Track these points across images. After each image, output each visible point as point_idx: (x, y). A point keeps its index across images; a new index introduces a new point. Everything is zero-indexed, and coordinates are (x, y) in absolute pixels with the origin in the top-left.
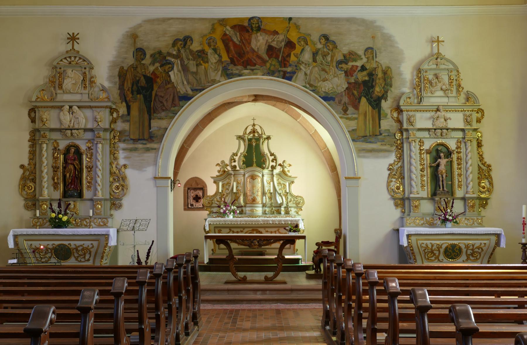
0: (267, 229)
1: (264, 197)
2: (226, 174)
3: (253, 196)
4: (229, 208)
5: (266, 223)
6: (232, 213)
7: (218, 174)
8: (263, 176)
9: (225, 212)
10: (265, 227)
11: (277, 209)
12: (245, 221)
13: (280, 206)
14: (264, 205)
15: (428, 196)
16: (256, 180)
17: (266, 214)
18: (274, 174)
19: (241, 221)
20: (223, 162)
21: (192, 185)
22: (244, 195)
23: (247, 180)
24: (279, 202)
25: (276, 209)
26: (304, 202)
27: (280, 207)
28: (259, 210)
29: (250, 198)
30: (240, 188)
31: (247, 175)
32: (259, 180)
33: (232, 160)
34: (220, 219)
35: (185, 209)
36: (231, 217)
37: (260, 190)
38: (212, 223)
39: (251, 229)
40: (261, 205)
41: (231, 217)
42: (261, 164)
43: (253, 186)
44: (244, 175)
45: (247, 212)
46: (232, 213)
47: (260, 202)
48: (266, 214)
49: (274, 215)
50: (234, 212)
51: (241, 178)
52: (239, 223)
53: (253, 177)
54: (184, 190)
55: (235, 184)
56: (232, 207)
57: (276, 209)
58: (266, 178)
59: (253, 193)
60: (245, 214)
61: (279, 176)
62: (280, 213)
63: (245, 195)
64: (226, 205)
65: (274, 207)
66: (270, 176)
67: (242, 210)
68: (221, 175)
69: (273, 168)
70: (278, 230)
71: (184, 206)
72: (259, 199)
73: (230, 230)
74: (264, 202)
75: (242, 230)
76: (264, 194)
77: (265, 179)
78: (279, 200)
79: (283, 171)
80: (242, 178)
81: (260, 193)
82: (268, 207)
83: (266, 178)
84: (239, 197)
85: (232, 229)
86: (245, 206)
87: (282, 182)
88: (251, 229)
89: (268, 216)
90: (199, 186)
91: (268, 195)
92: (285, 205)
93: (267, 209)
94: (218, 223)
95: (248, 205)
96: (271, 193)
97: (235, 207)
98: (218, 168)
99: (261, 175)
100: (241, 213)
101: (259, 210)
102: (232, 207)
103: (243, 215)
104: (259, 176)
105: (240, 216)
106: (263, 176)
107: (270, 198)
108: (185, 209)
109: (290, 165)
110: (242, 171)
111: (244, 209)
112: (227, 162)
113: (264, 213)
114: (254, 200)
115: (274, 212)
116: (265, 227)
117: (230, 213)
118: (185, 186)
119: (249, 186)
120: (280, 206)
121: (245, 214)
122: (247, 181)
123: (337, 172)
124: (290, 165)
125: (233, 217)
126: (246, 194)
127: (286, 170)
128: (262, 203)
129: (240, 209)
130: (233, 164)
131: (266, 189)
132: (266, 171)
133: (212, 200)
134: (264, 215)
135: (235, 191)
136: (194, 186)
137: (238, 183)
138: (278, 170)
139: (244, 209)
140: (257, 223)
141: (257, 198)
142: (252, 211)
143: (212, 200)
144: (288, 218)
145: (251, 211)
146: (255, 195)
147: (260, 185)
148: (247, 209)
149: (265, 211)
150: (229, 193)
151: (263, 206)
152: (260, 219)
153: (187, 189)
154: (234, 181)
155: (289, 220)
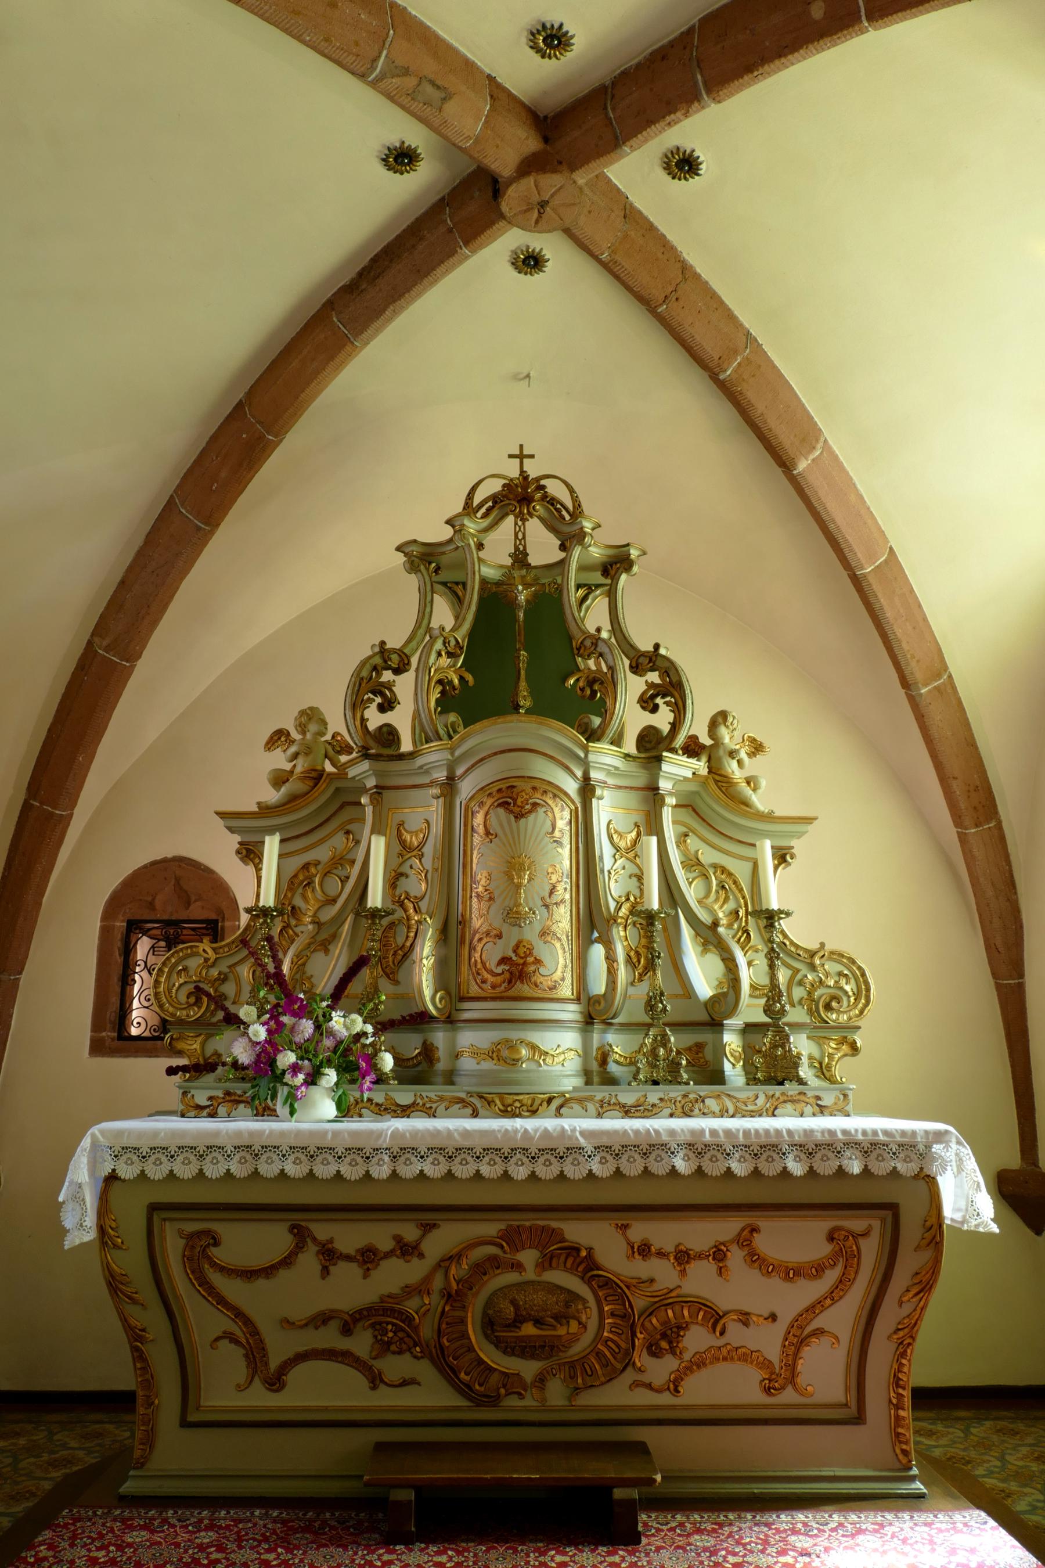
0: (641, 1230)
1: (598, 951)
2: (324, 793)
3: (512, 936)
4: (307, 1027)
5: (633, 1168)
6: (331, 1076)
7: (272, 796)
8: (587, 789)
9: (265, 1063)
10: (623, 1212)
11: (685, 1048)
12: (441, 1150)
13: (713, 1017)
14: (594, 1013)
15: (209, 1058)
16: (537, 821)
17: (610, 1081)
18: (665, 785)
19: (401, 1151)
20: (310, 716)
21: (151, 906)
22: (444, 934)
23: (469, 814)
24: (704, 987)
25: (689, 1039)
26: (863, 990)
27: (716, 1025)
28: (559, 1051)
29: (490, 953)
30: (415, 885)
31: (466, 788)
32: (563, 818)
33: (370, 686)
34: (242, 1125)
35: (98, 1048)
36: (321, 1107)
37: (564, 892)
38: (127, 1172)
39: (491, 1229)
40: (571, 1012)
41: (321, 1107)
42: (584, 708)
43: (514, 867)
44: (450, 785)
45: (467, 1064)
46: (331, 1076)
47: (566, 990)
48: (610, 1081)
49: (675, 1092)
50: (352, 1061)
51: (424, 812)
52: (381, 1170)
53: (515, 799)
54: (105, 932)
55: (378, 847)
56: (338, 1022)
57: (689, 1039)
58: (609, 811)
59: (514, 916)
60: (450, 1078)
61: (685, 816)
62: (717, 1077)
63: (453, 933)
64: (286, 998)
65: (676, 1026)
66: (633, 800)
67: (428, 1052)
68: (293, 800)
69: (652, 746)
70: (745, 1239)
71: (97, 1024)
72: (557, 964)
73: (301, 1235)
74: (598, 986)
75: (410, 1232)
76: (593, 922)
77: (595, 818)
78: (702, 975)
79: (717, 775)
80: (435, 810)
81: (563, 919)
82: (628, 1027)
83: (609, 811)
84: (406, 953)
85: (322, 1231)
86: (450, 1020)
87: (708, 856)
88: (491, 1229)
89: (628, 1098)
90: (198, 911)
91: (623, 940)
92: (751, 1010)
93: (619, 1044)
94: (185, 1171)
95: (472, 1011)
96: (650, 917)
97: (358, 1024)
98: (279, 760)
99: (571, 786)
100: (417, 1070)
101: (559, 1051)
102: (338, 1022)
103: (429, 1092)
104: (558, 793)
105: (404, 1096)
106: (587, 789)
107: (644, 961)
108: (98, 1048)
109: (757, 748)
110: (435, 758)
111: (439, 1038)
112: (337, 723)
113: (598, 1071)
114: (518, 971)
115: (674, 1067)
116: (623, 1212)
117: (312, 1080)
118: (114, 904)
119: (482, 864)
120: (713, 1017)
121: (450, 1078)
122: (469, 829)
123: (999, 826)
124: (757, 748)
125: (345, 1110)
126: (463, 922)
127: (732, 767)
128: (582, 994)
129: (411, 1043)
130: (375, 719)
131: (615, 887)
132: (605, 758)
133: (223, 978)
134: (601, 1093)
135: (376, 898)
136: (166, 907)
137: (403, 851)
138: (678, 770)
139: (439, 1038)
140: (546, 1172)
141: (541, 950)
142: (504, 1055)
143: (223, 978)
144: (788, 1123)
145: (494, 1053)
146: (530, 934)
147: (564, 857)
148: (468, 1038)
149: (604, 1061)
150: (338, 920)
151: (588, 1020)
152: (579, 1125)
153: (120, 924)
154: (376, 830)
155: (851, 1143)
